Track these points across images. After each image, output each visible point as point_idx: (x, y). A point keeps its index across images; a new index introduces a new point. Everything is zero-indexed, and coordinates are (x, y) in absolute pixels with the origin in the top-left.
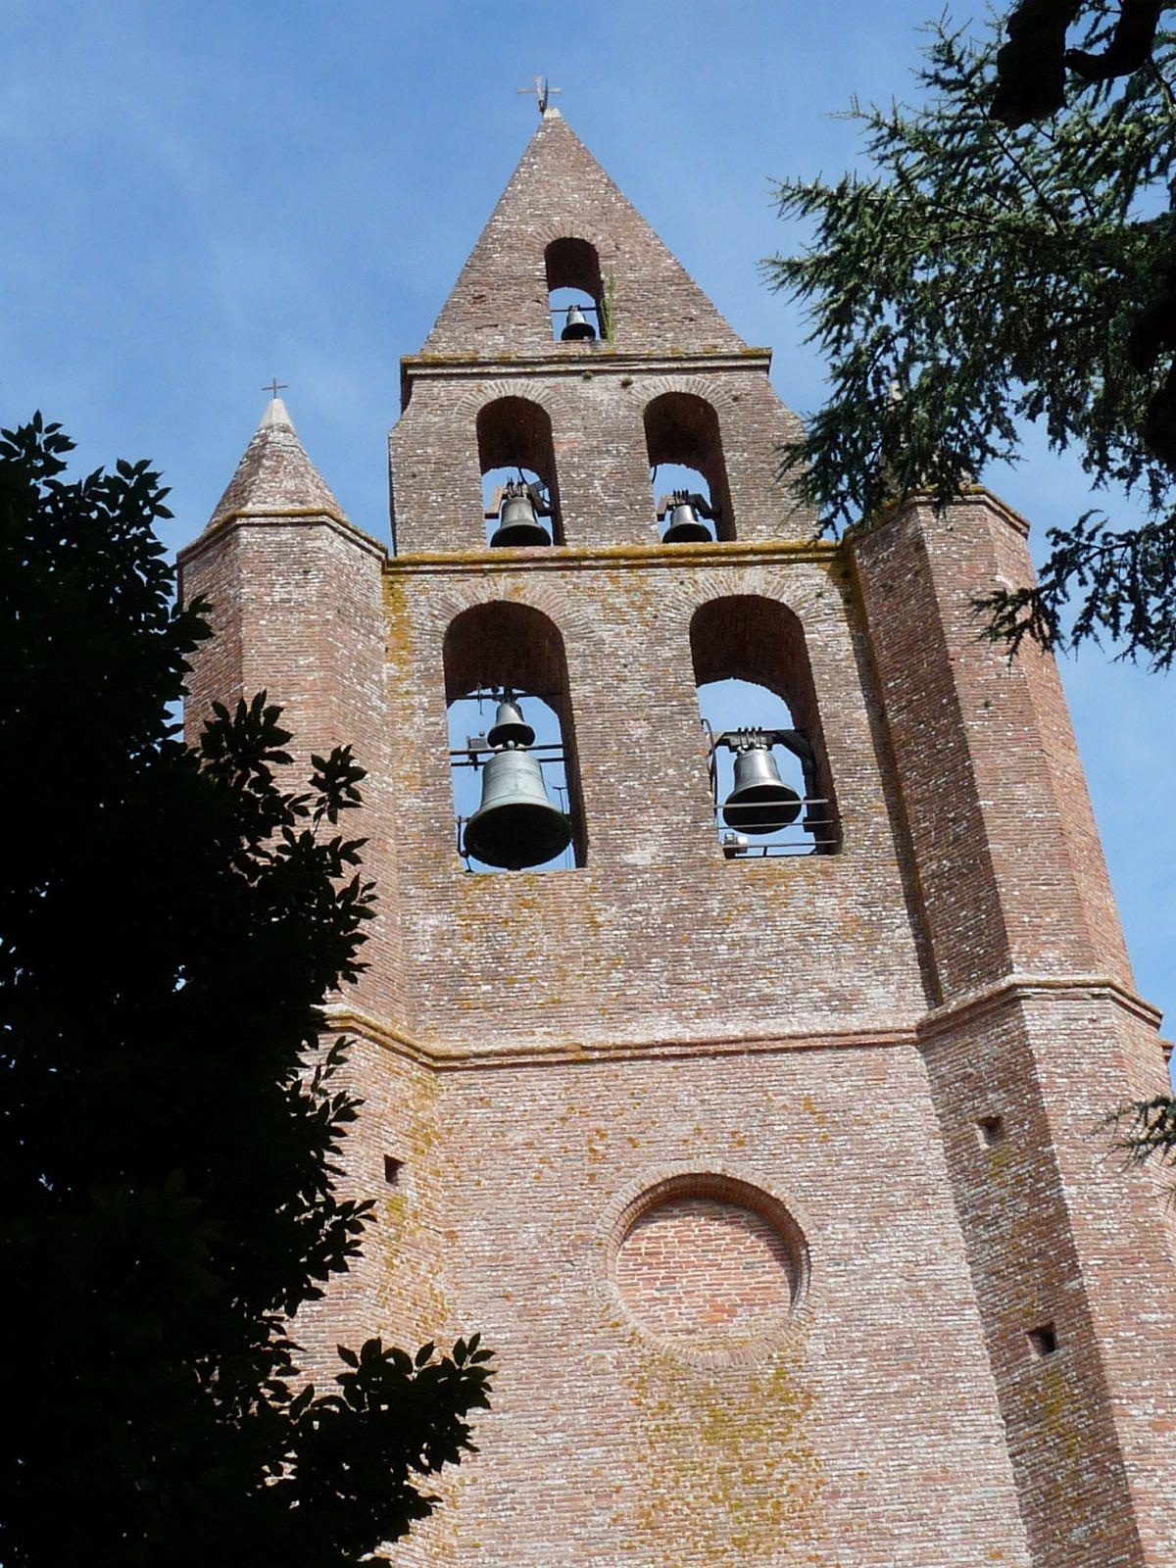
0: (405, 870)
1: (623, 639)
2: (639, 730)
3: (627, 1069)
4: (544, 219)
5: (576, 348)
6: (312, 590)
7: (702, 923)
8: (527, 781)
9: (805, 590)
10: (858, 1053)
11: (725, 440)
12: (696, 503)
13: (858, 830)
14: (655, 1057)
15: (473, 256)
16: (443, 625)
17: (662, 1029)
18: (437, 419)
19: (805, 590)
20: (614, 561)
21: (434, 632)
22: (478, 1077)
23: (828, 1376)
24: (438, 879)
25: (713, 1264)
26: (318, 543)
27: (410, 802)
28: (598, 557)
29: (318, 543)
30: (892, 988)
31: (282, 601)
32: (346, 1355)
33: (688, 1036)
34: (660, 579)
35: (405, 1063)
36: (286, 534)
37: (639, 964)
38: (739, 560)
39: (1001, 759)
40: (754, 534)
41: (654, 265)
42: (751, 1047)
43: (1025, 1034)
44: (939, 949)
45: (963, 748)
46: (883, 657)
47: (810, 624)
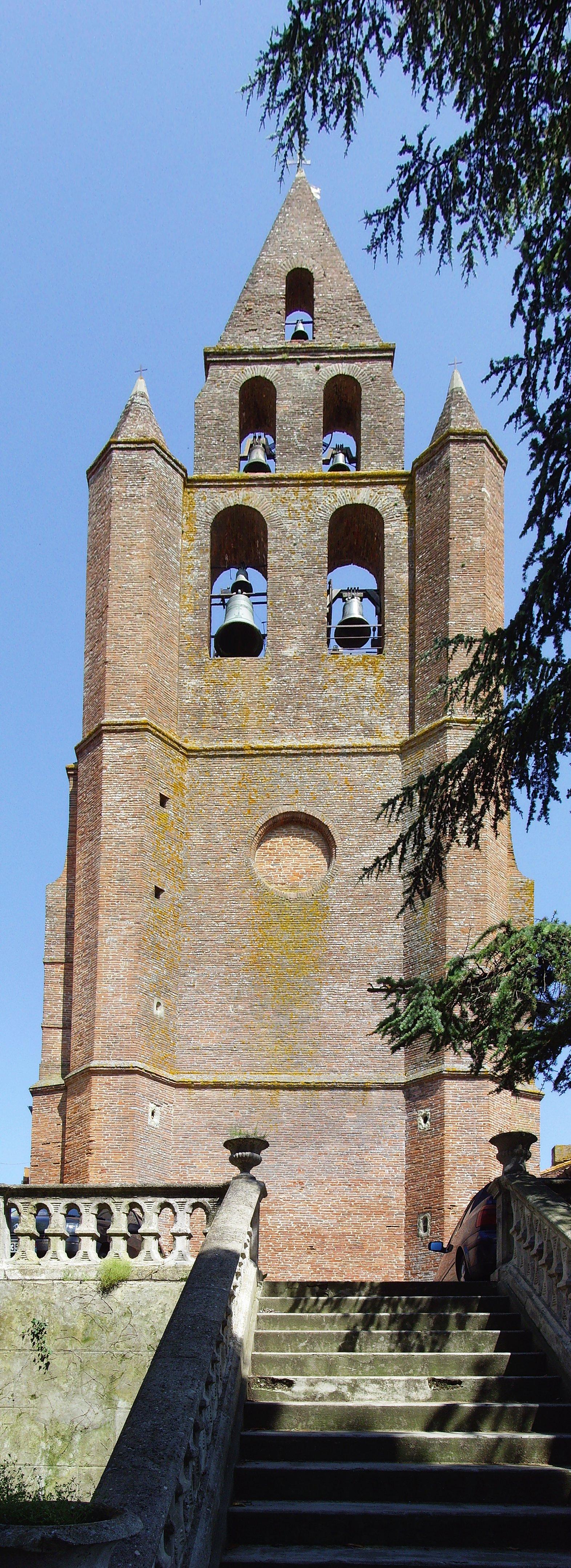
0: (182, 655)
1: (296, 528)
3: (270, 761)
5: (297, 344)
8: (242, 611)
9: (388, 501)
10: (372, 758)
11: (363, 406)
12: (347, 452)
13: (391, 642)
14: (283, 755)
15: (248, 280)
16: (211, 518)
17: (290, 741)
18: (219, 391)
24: (197, 660)
26: (150, 461)
27: (188, 619)
28: (290, 479)
29: (150, 461)
30: (394, 726)
31: (131, 496)
35: (173, 751)
36: (135, 455)
37: (281, 708)
38: (358, 482)
39: (464, 599)
41: (343, 287)
43: (445, 746)
44: (418, 704)
45: (447, 591)
46: (419, 540)
47: (387, 522)
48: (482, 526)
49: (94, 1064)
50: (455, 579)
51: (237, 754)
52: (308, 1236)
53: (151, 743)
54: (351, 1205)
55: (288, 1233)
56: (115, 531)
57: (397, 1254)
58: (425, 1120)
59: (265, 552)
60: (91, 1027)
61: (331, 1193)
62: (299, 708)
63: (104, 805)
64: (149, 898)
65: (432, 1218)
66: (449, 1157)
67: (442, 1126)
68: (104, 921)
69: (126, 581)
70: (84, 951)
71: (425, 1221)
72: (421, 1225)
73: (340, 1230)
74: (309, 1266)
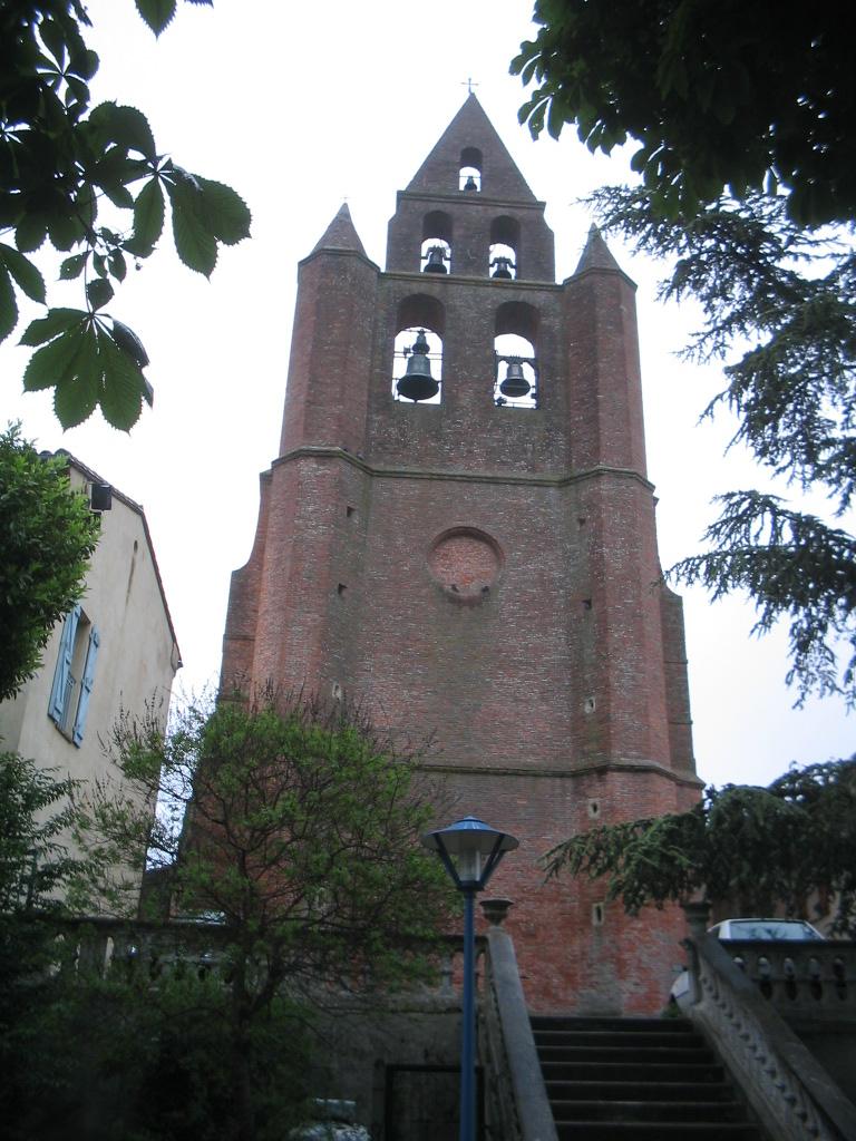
25: (468, 561)
54: (524, 892)
58: (595, 808)
62: (472, 444)
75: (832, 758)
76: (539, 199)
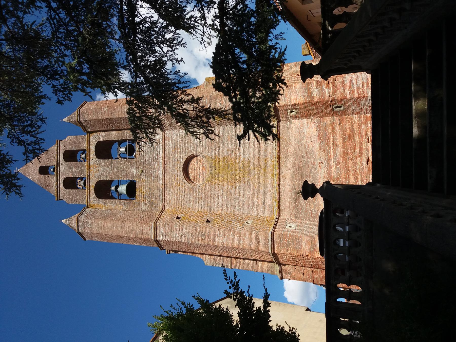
2: (115, 170)
3: (166, 179)
4: (36, 174)
6: (89, 221)
7: (145, 163)
8: (123, 189)
9: (95, 139)
16: (98, 199)
19: (95, 139)
20: (89, 170)
21: (99, 201)
22: (166, 202)
23: (213, 154)
25: (196, 168)
32: (286, 59)
33: (162, 168)
34: (92, 163)
35: (163, 214)
36: (80, 224)
37: (151, 175)
38: (89, 150)
39: (120, 112)
40: (85, 147)
42: (164, 159)
45: (118, 118)
46: (104, 129)
48: (101, 108)
49: (270, 252)
50: (115, 116)
51: (164, 190)
52: (344, 159)
53: (160, 222)
55: (343, 169)
56: (100, 232)
57: (352, 119)
59: (106, 180)
60: (256, 251)
61: (324, 150)
62: (151, 168)
63: (179, 241)
64: (210, 224)
65: (335, 105)
66: (308, 100)
67: (295, 104)
68: (218, 243)
69: (113, 229)
70: (227, 252)
71: (336, 107)
72: (338, 109)
73: (341, 145)
74: (358, 158)
75: (319, 209)
76: (310, 198)
